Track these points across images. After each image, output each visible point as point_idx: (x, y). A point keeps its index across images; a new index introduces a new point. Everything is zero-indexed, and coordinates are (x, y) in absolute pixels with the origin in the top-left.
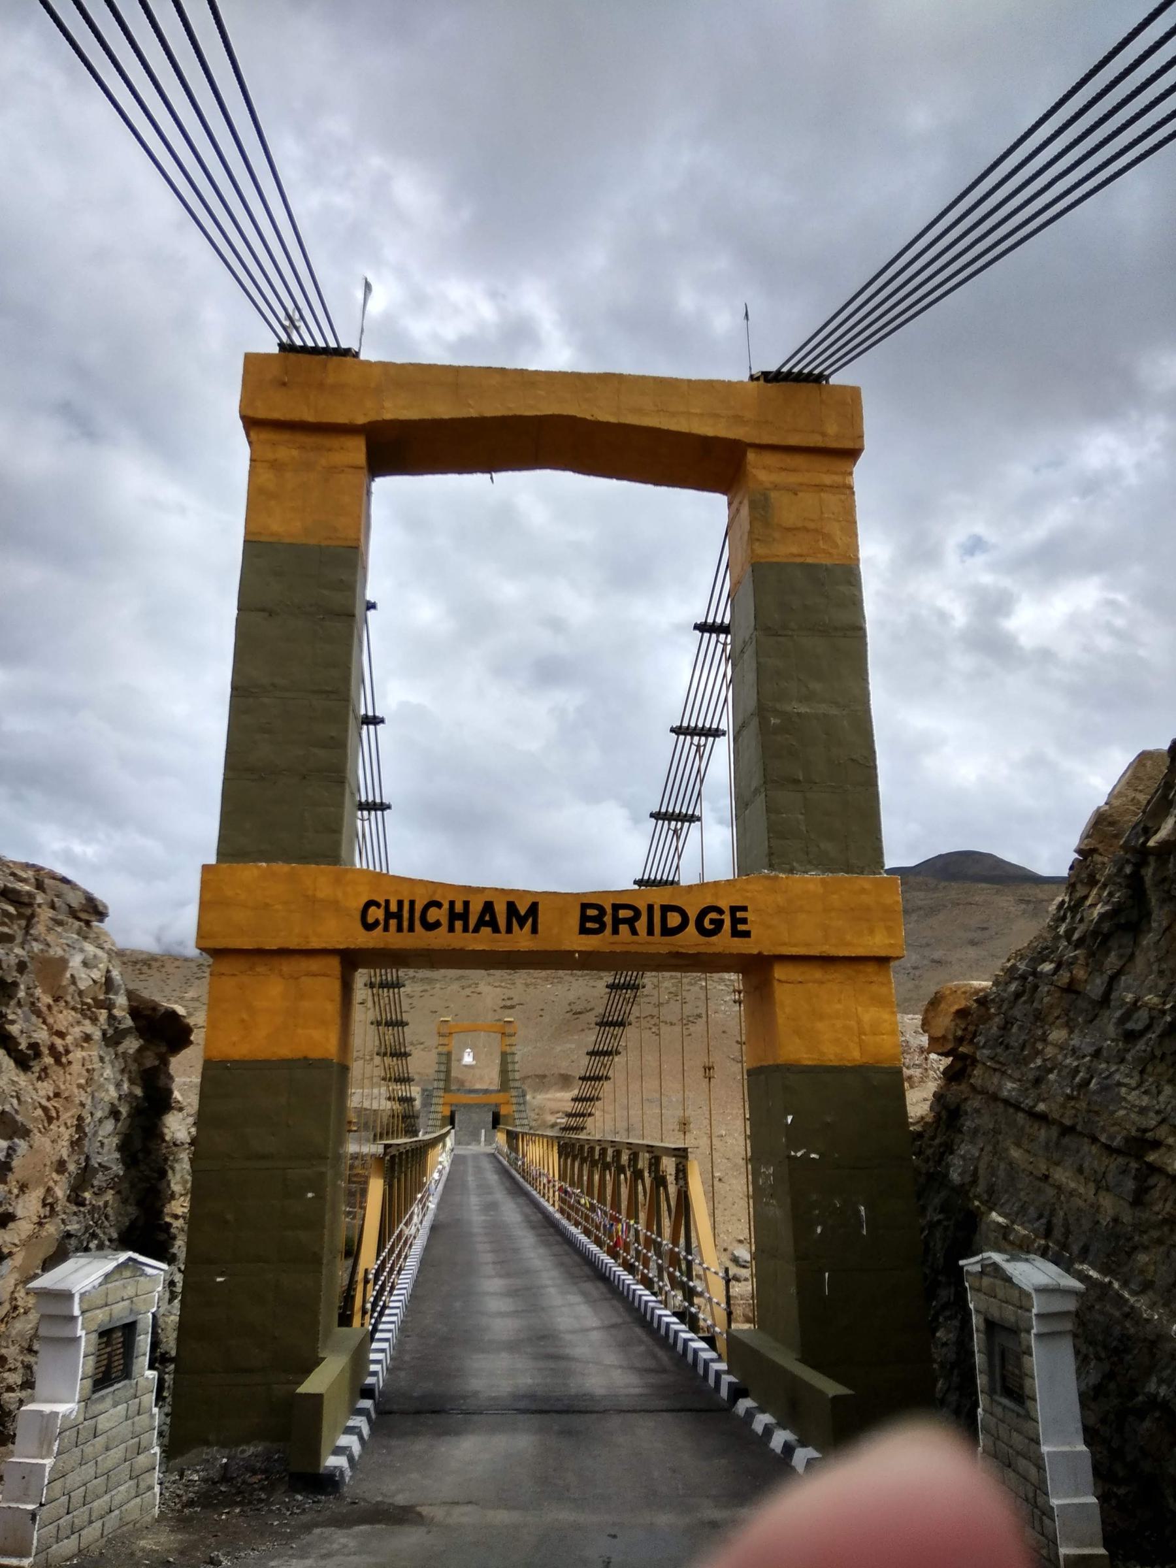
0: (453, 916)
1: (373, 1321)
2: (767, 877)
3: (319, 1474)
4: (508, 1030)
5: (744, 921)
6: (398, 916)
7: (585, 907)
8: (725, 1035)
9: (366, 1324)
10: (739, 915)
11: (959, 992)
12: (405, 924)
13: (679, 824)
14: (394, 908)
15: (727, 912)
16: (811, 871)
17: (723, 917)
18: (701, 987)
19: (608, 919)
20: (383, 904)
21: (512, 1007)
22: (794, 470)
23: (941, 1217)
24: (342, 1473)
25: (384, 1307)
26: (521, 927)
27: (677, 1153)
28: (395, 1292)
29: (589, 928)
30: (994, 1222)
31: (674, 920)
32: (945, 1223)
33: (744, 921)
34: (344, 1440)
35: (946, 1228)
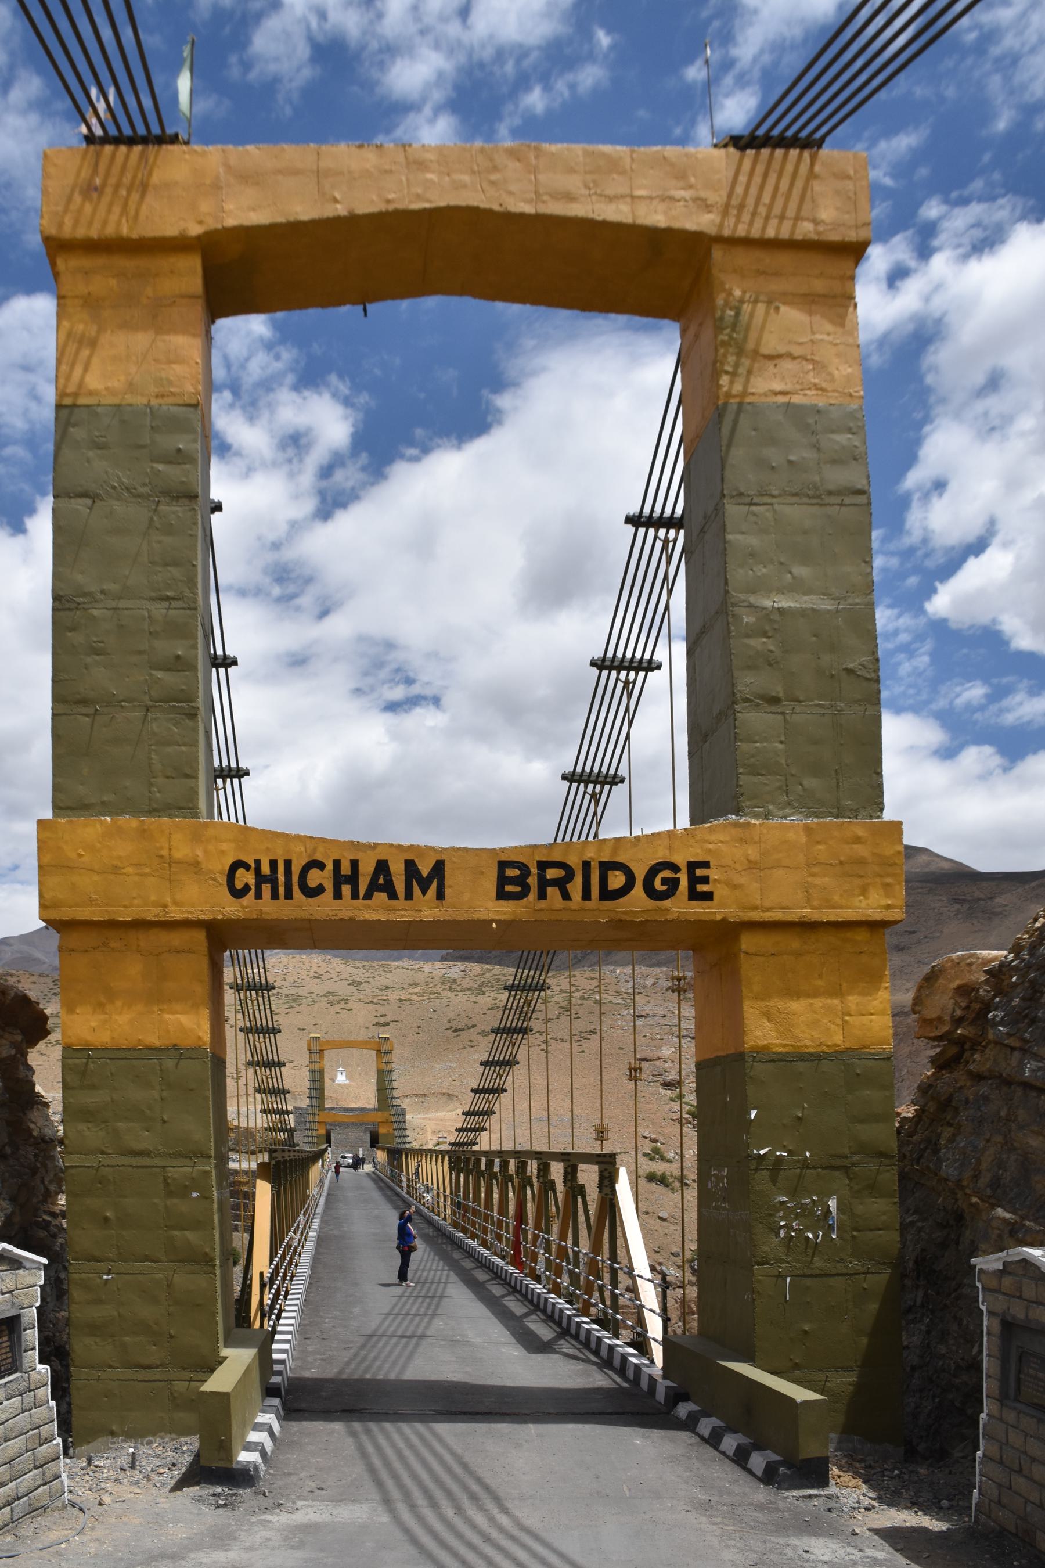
0: (339, 880)
1: (271, 1323)
2: (736, 825)
3: (233, 1468)
4: (385, 1047)
5: (705, 880)
6: (273, 880)
7: (503, 865)
8: (622, 1051)
9: (266, 1327)
10: (699, 872)
11: (962, 964)
12: (282, 890)
13: (598, 787)
14: (266, 869)
15: (684, 870)
16: (790, 816)
17: (678, 876)
18: (596, 1002)
19: (532, 881)
20: (253, 865)
21: (387, 1024)
22: (776, 274)
23: (915, 1218)
24: (256, 1468)
25: (281, 1311)
26: (424, 892)
27: (601, 1159)
28: (289, 1297)
29: (509, 892)
30: (999, 1218)
31: (617, 880)
32: (920, 1224)
33: (705, 880)
34: (254, 1437)
35: (920, 1230)
